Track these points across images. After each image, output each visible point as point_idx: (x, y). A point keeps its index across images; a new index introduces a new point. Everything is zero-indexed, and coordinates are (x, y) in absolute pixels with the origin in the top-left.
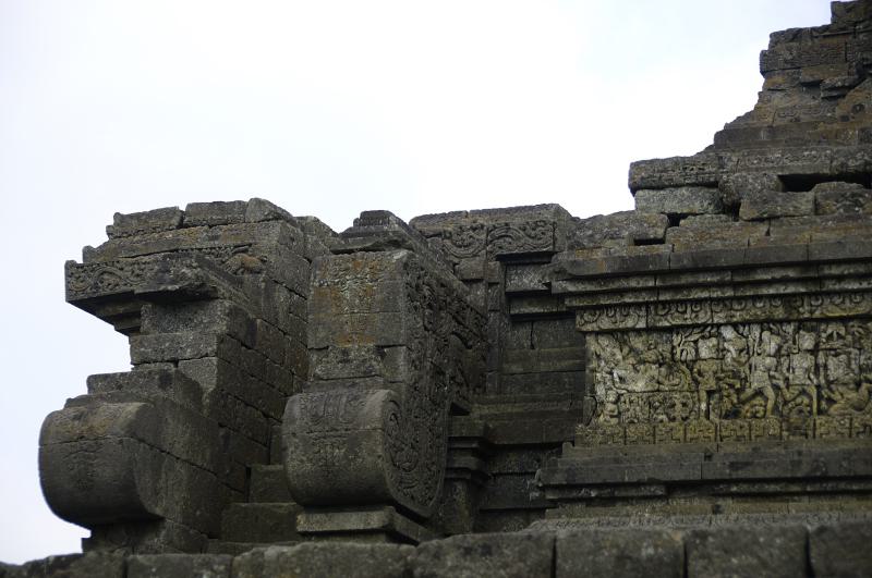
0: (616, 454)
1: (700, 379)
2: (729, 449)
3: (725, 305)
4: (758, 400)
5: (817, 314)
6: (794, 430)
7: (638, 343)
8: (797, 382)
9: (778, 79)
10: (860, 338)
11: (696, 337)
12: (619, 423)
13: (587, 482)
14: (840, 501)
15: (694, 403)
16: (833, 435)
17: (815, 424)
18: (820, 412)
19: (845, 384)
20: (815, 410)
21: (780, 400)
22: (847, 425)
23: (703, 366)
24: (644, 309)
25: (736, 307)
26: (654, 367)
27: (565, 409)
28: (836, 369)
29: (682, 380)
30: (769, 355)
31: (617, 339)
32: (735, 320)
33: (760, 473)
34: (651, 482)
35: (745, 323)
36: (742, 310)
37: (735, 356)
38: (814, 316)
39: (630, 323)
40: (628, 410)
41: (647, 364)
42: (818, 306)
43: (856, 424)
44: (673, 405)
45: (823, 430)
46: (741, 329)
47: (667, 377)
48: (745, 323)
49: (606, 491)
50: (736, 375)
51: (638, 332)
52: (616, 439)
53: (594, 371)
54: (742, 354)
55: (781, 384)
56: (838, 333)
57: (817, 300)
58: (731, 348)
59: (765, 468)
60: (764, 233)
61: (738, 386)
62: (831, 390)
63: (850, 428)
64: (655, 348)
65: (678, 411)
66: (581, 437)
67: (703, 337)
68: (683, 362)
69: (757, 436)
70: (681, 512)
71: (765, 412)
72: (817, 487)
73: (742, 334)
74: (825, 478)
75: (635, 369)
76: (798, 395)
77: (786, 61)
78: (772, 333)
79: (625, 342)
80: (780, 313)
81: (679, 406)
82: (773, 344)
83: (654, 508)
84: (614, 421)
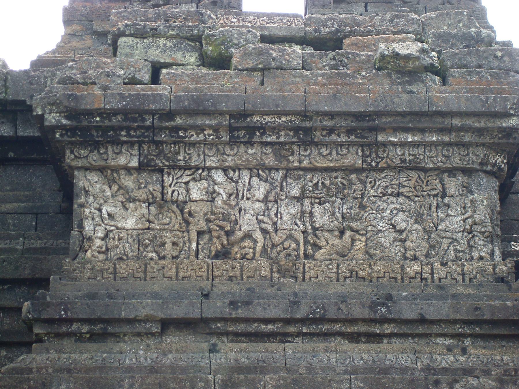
0: (107, 290)
1: (191, 219)
2: (223, 288)
3: (218, 150)
4: (247, 243)
5: (305, 163)
6: (283, 272)
7: (128, 182)
8: (285, 227)
9: (75, 27)
10: (344, 189)
11: (188, 178)
12: (107, 259)
13: (81, 316)
14: (333, 343)
15: (184, 243)
16: (321, 278)
17: (304, 268)
18: (306, 256)
19: (330, 231)
20: (302, 255)
21: (269, 243)
22: (335, 270)
23: (194, 207)
24: (136, 147)
25: (228, 152)
26: (144, 205)
27: (19, 247)
28: (321, 216)
29: (173, 219)
30: (258, 201)
31: (106, 177)
32: (227, 164)
33: (260, 313)
34: (147, 320)
35: (237, 168)
36: (234, 155)
37: (225, 199)
38: (303, 165)
39: (122, 161)
40: (117, 247)
41: (138, 203)
42: (305, 156)
43: (343, 269)
44: (163, 244)
45: (312, 273)
46: (231, 173)
47: (156, 216)
48: (237, 168)
49: (98, 327)
50: (225, 218)
51: (128, 170)
52: (105, 275)
53: (82, 206)
54: (232, 198)
55: (270, 228)
56: (322, 183)
57: (306, 150)
58: (222, 191)
59: (265, 309)
60: (258, 83)
61: (228, 228)
62: (316, 236)
63: (338, 273)
64: (145, 187)
65: (169, 250)
66: (68, 271)
67: (194, 179)
68: (173, 202)
69: (248, 277)
70: (177, 350)
71: (254, 254)
72: (313, 329)
73: (232, 179)
74: (322, 320)
75: (124, 206)
76: (286, 240)
77: (82, 16)
78: (260, 180)
79: (114, 181)
80: (270, 160)
81: (169, 246)
82: (262, 190)
83: (148, 345)
84: (102, 257)
